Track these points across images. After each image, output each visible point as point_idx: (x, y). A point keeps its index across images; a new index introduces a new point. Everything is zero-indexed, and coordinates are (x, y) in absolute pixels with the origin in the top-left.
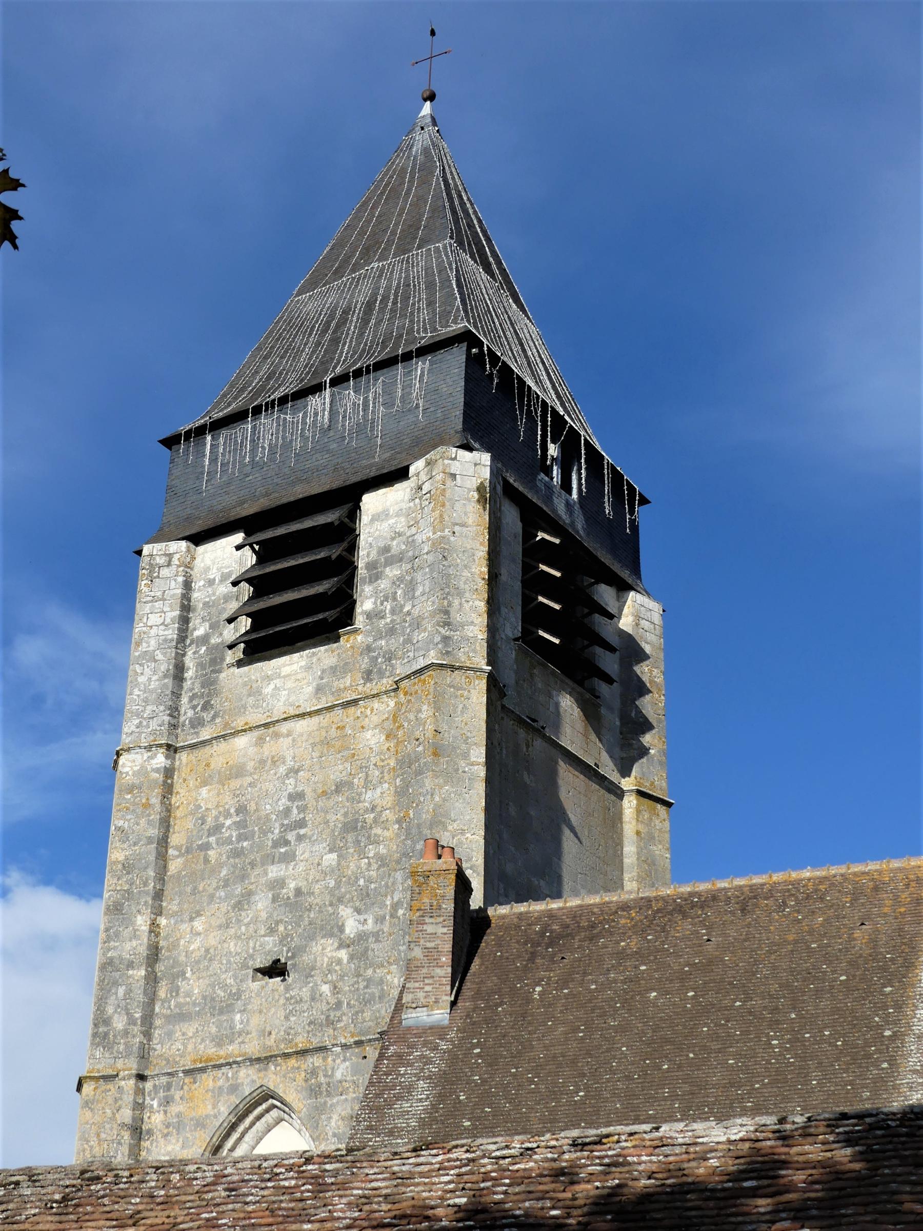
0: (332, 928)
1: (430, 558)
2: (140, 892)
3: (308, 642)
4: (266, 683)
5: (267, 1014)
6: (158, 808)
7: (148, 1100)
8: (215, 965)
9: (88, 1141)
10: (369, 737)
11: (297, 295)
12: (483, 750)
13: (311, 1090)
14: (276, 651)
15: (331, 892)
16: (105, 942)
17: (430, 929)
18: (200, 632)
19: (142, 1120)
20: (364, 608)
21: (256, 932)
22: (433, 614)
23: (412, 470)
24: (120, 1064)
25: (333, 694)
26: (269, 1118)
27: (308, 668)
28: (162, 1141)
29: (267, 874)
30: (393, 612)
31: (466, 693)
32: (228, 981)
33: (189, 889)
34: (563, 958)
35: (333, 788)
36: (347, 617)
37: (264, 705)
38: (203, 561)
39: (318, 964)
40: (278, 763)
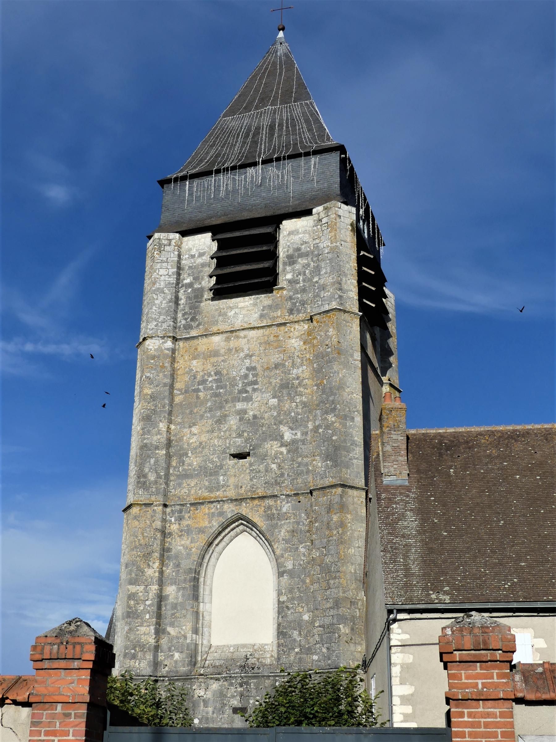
0: (276, 436)
1: (330, 256)
2: (161, 411)
3: (255, 291)
4: (229, 310)
5: (237, 477)
6: (169, 368)
7: (168, 517)
8: (206, 451)
9: (137, 537)
10: (293, 342)
11: (224, 117)
12: (359, 354)
13: (268, 517)
14: (235, 295)
15: (275, 418)
16: (142, 435)
17: (394, 437)
18: (188, 281)
19: (165, 527)
20: (287, 278)
21: (230, 435)
22: (333, 284)
23: (314, 211)
24: (153, 498)
25: (270, 319)
26: (238, 530)
27: (255, 305)
28: (178, 539)
29: (235, 407)
30: (304, 281)
31: (351, 325)
32: (215, 459)
33: (188, 411)
34: (459, 456)
35: (273, 366)
36: (275, 282)
37: (229, 321)
38: (187, 245)
39: (269, 454)
40: (239, 351)
